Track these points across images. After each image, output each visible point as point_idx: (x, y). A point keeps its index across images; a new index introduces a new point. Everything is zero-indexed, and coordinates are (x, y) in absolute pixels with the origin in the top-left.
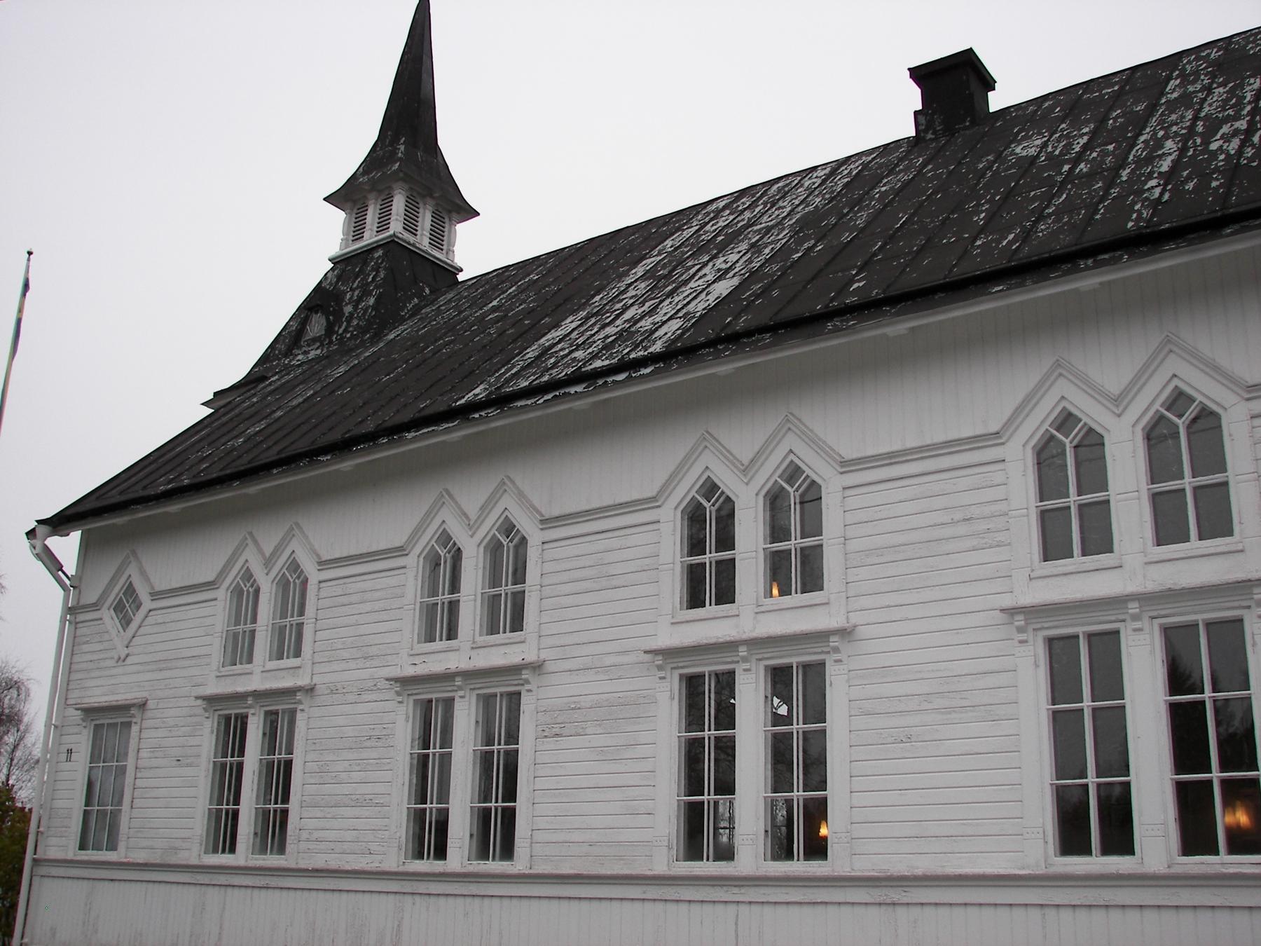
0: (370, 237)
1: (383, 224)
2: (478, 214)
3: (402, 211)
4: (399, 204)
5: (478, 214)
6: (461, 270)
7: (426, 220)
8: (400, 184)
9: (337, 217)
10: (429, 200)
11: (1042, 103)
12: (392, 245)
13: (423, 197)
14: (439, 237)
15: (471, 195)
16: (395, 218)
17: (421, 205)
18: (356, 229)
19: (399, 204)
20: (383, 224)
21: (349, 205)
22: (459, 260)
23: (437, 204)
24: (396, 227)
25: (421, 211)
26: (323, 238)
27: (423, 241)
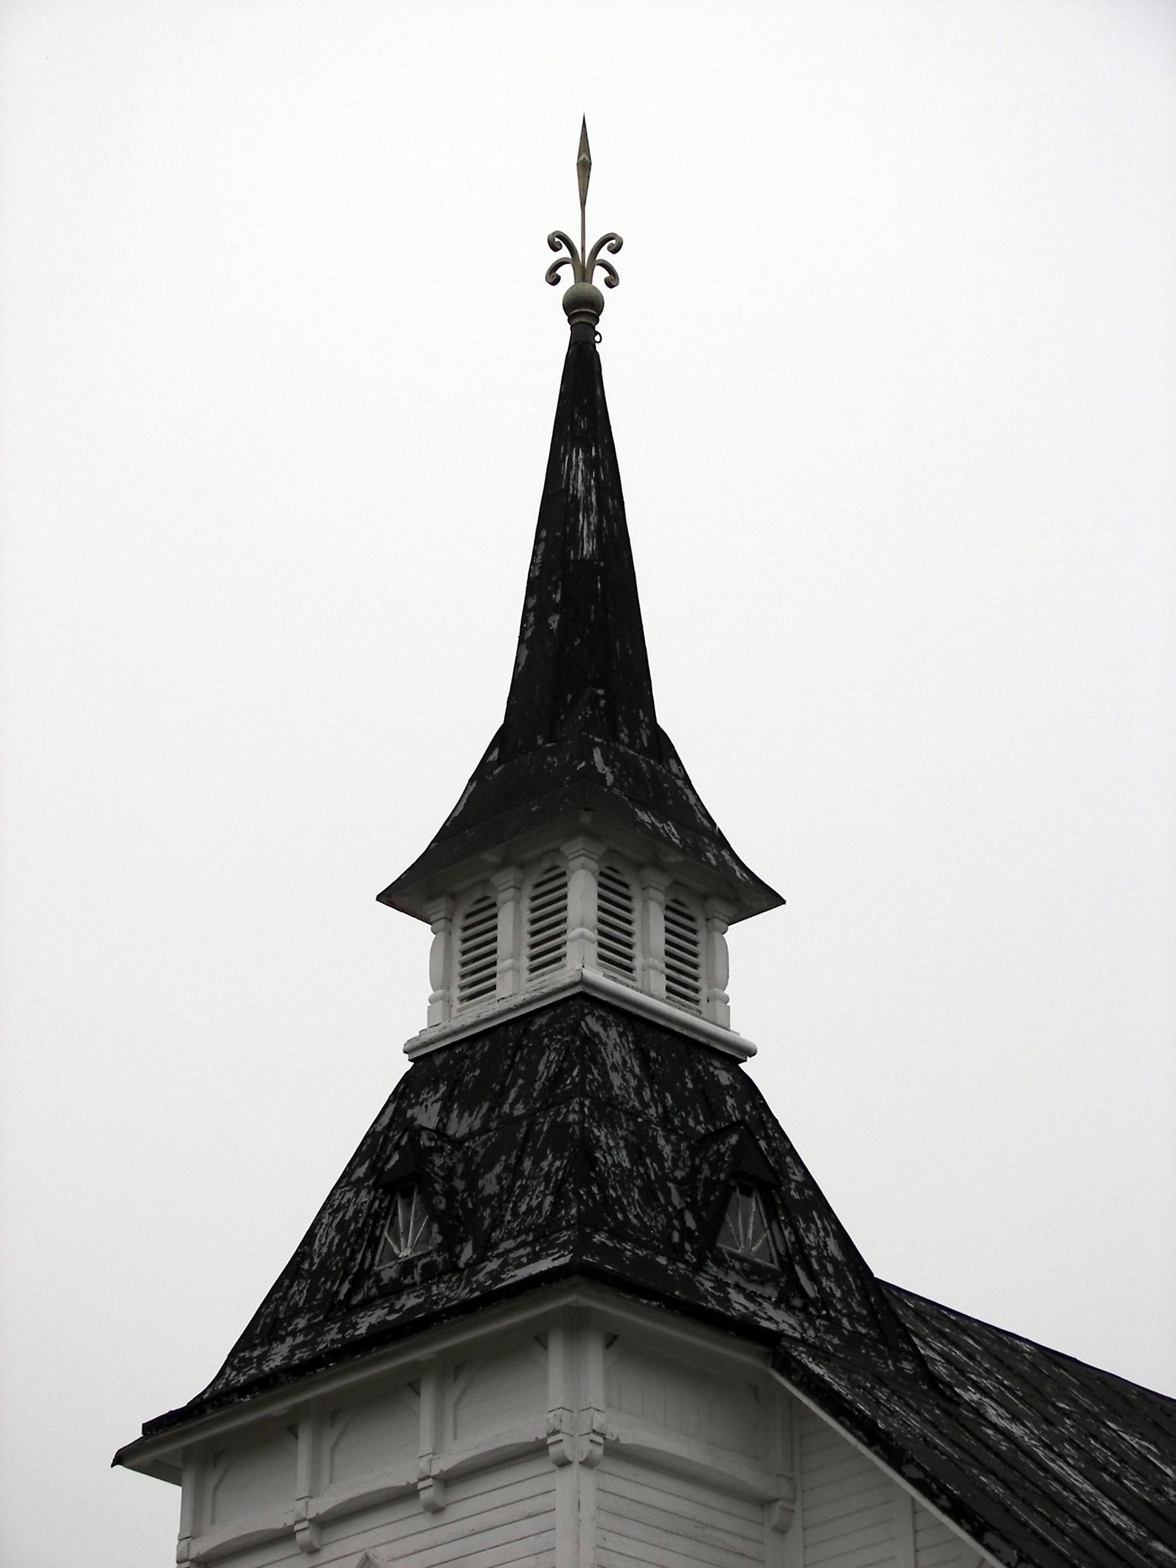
0: (515, 986)
1: (546, 950)
2: (784, 902)
3: (593, 914)
4: (582, 896)
6: (751, 1053)
7: (651, 930)
8: (578, 844)
9: (414, 939)
10: (651, 875)
11: (531, 1023)
12: (585, 998)
13: (639, 867)
14: (690, 969)
16: (577, 939)
17: (634, 891)
18: (471, 965)
19: (582, 896)
20: (546, 950)
21: (440, 907)
22: (742, 1023)
23: (677, 883)
24: (581, 962)
25: (636, 904)
26: (374, 1003)
27: (647, 990)
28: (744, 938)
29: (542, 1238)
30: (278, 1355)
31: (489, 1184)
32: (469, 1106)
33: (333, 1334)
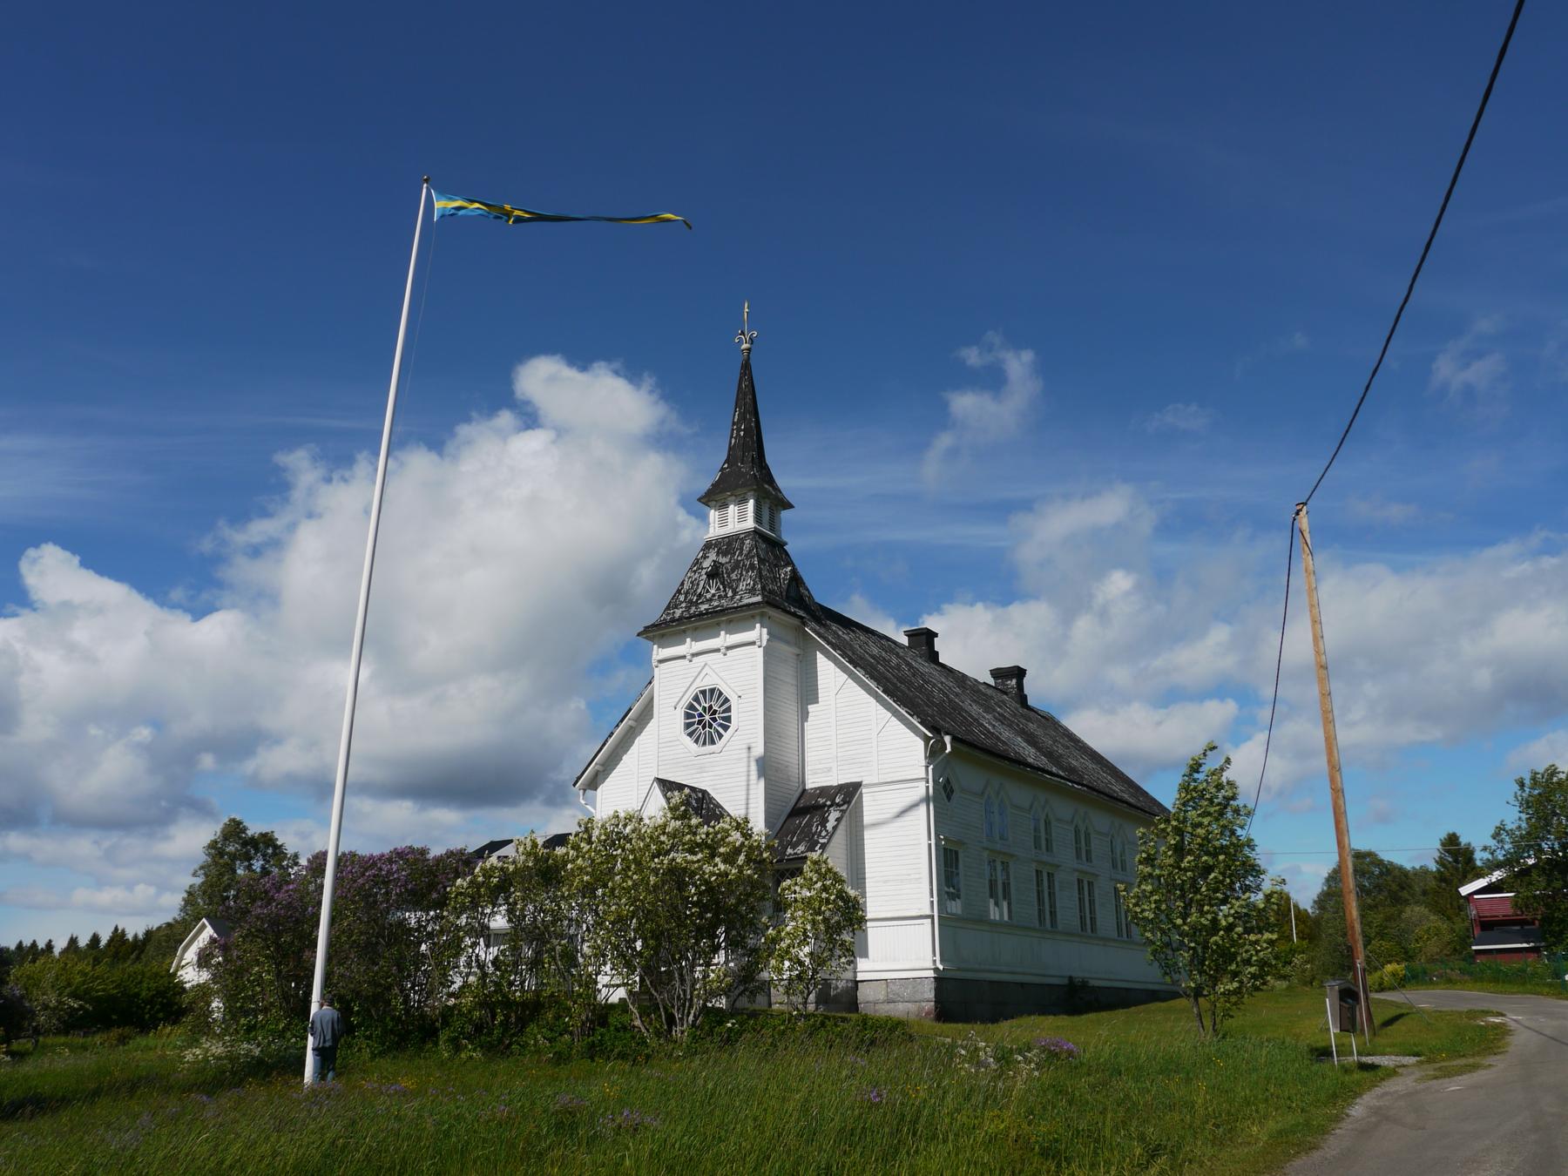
2: (791, 506)
5: (791, 506)
15: (788, 495)
22: (785, 538)
28: (785, 515)
29: (752, 592)
30: (678, 613)
31: (734, 576)
32: (725, 555)
33: (693, 609)
